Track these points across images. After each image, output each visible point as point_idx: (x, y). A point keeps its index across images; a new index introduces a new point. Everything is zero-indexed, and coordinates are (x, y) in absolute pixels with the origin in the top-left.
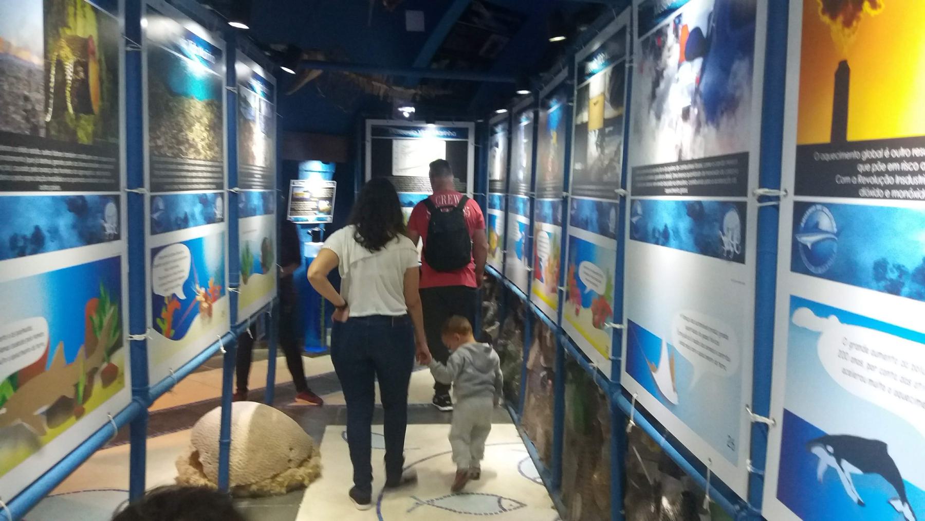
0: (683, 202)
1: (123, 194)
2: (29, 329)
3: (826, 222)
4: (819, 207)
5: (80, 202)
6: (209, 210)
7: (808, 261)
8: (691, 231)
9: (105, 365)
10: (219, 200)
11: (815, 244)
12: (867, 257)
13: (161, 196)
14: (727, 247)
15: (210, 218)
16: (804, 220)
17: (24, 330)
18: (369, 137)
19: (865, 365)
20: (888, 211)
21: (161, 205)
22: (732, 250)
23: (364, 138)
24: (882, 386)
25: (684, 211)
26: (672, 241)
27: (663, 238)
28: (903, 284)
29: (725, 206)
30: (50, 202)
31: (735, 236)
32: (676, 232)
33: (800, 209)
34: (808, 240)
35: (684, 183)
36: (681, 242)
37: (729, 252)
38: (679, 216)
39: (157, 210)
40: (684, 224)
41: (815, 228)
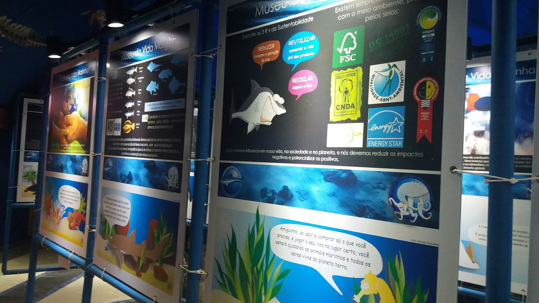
0: (142, 161)
1: (91, 156)
2: (480, 239)
3: (236, 174)
4: (232, 167)
5: (152, 164)
6: (77, 166)
7: (226, 191)
8: (147, 176)
9: (158, 264)
10: (85, 161)
11: (229, 184)
12: (258, 187)
13: (110, 158)
14: (170, 185)
15: (77, 171)
16: (224, 173)
17: (482, 239)
18: (25, 111)
19: (298, 232)
20: (284, 169)
21: (111, 164)
22: (173, 186)
23: (21, 111)
24: (521, 232)
25: (143, 165)
26: (134, 181)
27: (128, 179)
28: (274, 199)
29: (170, 165)
30: (136, 162)
31: (175, 180)
32: (137, 176)
33: (223, 167)
34: (227, 182)
35: (483, 165)
36: (140, 181)
37: (171, 187)
38: (139, 168)
39: (108, 166)
40: (143, 173)
41: (231, 177)
